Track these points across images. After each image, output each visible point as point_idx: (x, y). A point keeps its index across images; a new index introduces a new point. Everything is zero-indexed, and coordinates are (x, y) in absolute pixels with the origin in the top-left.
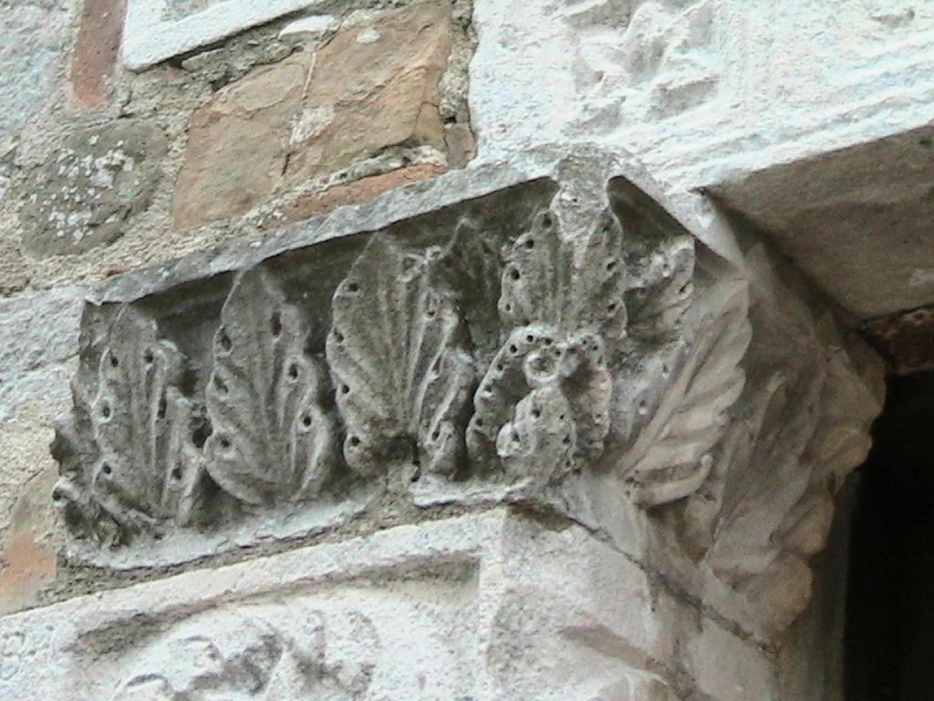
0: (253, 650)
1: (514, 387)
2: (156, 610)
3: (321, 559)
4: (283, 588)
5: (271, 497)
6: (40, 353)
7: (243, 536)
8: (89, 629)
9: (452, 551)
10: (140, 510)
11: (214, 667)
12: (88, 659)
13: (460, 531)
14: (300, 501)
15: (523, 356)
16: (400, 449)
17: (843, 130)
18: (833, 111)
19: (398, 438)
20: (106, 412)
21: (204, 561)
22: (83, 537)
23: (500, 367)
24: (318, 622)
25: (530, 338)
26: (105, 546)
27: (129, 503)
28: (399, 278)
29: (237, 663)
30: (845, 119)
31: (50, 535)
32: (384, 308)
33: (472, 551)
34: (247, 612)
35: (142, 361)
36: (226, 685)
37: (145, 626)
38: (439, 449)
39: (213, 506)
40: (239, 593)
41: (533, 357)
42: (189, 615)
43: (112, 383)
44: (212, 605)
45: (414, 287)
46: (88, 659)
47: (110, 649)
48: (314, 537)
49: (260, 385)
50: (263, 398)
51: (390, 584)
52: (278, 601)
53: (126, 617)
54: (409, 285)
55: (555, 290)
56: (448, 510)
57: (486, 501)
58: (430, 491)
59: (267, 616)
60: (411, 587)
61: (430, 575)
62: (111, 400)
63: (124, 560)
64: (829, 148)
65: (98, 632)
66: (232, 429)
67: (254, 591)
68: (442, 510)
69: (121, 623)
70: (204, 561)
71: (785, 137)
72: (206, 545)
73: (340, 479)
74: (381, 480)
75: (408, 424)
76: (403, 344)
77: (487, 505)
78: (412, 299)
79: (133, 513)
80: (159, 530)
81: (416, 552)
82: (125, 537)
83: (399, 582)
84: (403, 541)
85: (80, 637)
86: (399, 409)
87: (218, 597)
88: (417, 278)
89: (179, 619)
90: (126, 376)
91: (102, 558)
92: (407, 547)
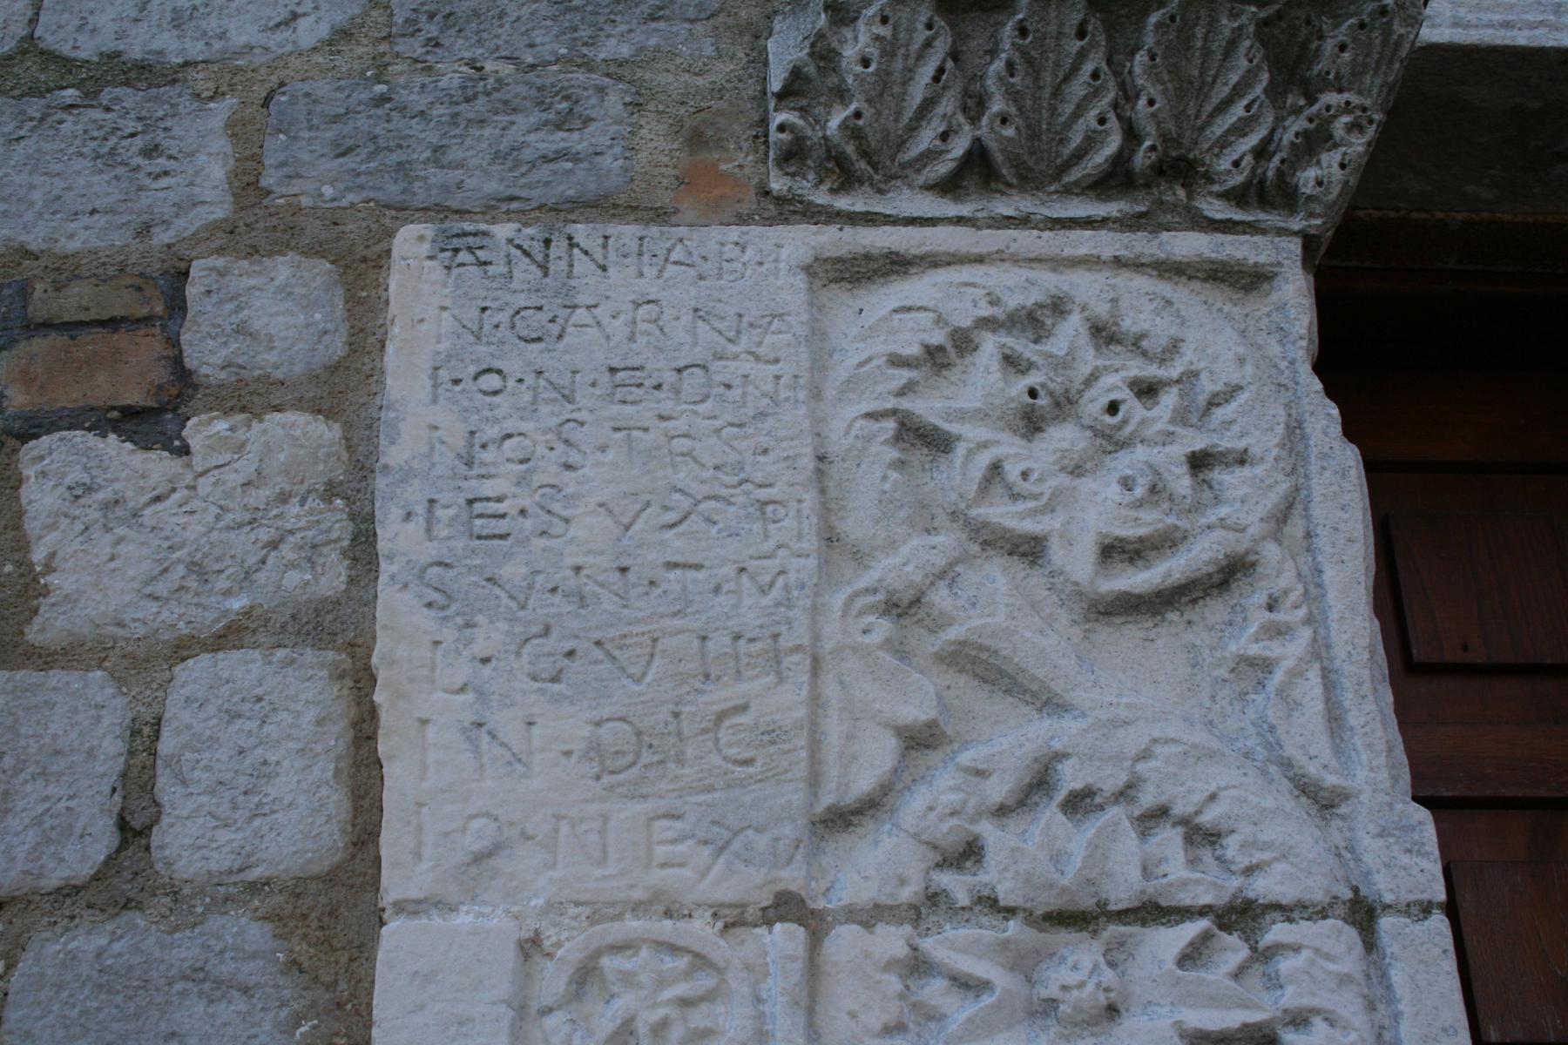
0: (1041, 306)
1: (1315, 141)
2: (914, 251)
3: (1083, 243)
4: (1064, 259)
5: (1027, 180)
6: (661, 8)
7: (1004, 207)
8: (828, 254)
9: (1251, 262)
10: (869, 163)
11: (999, 313)
12: (818, 283)
13: (1256, 247)
14: (1056, 192)
15: (1335, 117)
16: (1180, 168)
17: (1502, 32)
18: (1497, 18)
19: (1178, 159)
20: (866, 63)
21: (960, 221)
22: (793, 175)
23: (1311, 120)
24: (1112, 294)
25: (1348, 103)
26: (824, 188)
27: (865, 154)
28: (1224, 21)
29: (1024, 312)
30: (1507, 25)
31: (740, 166)
32: (1199, 44)
33: (1272, 265)
34: (1024, 273)
35: (920, 26)
36: (1003, 331)
37: (897, 265)
38: (1231, 163)
39: (976, 173)
40: (1012, 255)
41: (1346, 119)
42: (949, 264)
43: (877, 38)
44: (980, 260)
45: (1237, 35)
46: (818, 283)
47: (843, 279)
48: (1088, 223)
49: (1047, 78)
50: (1048, 90)
51: (1176, 279)
52: (1054, 270)
53: (875, 252)
54: (1233, 30)
55: (1377, 69)
56: (1240, 228)
57: (1281, 228)
58: (1217, 209)
59: (1049, 282)
60: (1196, 285)
61: (1215, 279)
62: (874, 52)
63: (843, 203)
64: (1499, 42)
65: (839, 260)
66: (1013, 110)
67: (1033, 255)
68: (1227, 227)
69: (868, 257)
70: (960, 221)
71: (1455, 25)
72: (950, 209)
73: (1115, 179)
74: (1155, 191)
75: (1190, 150)
76: (1210, 79)
77: (1281, 232)
78: (1232, 45)
79: (863, 165)
80: (883, 186)
81: (1213, 255)
82: (847, 180)
83: (1184, 279)
84: (1189, 245)
85: (817, 259)
86: (1188, 134)
87: (989, 254)
88: (1241, 28)
89: (935, 265)
90: (895, 36)
91: (821, 197)
92: (1202, 250)
